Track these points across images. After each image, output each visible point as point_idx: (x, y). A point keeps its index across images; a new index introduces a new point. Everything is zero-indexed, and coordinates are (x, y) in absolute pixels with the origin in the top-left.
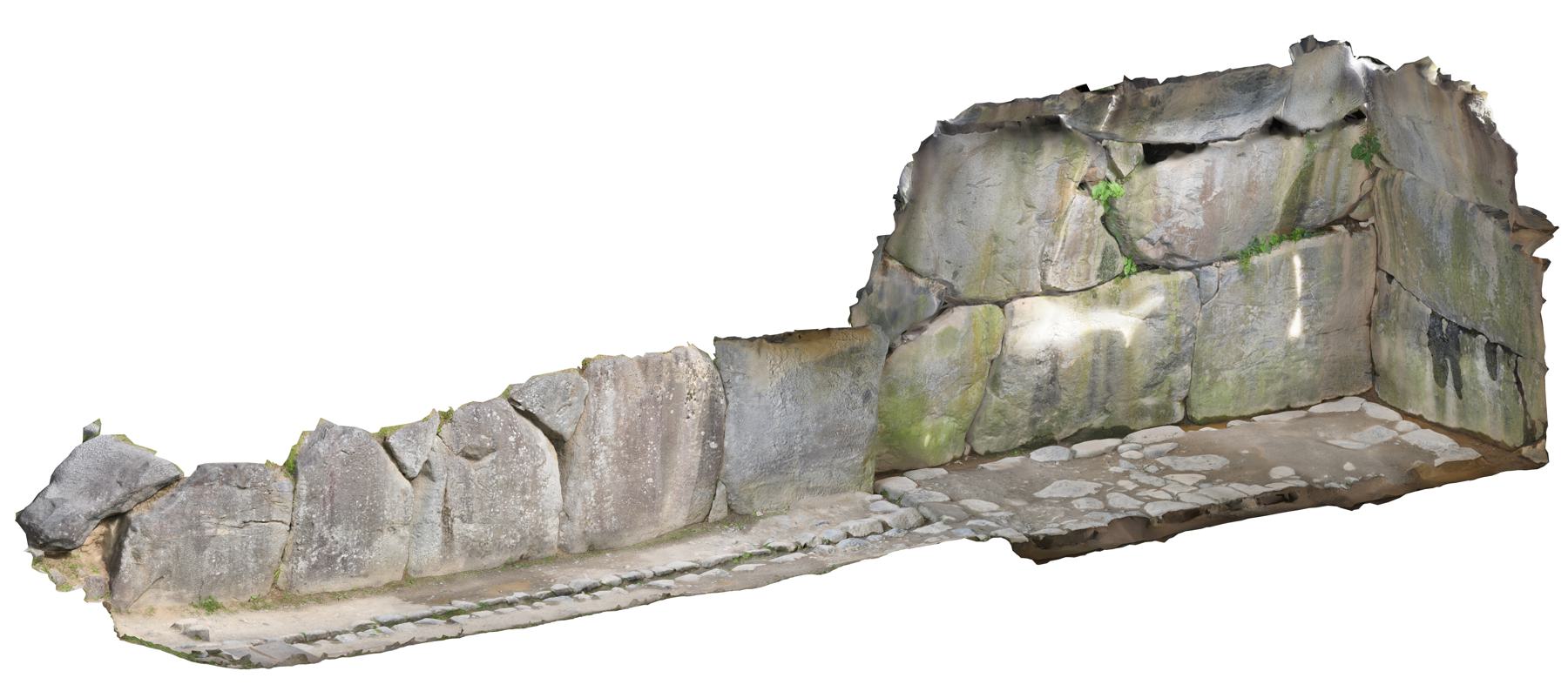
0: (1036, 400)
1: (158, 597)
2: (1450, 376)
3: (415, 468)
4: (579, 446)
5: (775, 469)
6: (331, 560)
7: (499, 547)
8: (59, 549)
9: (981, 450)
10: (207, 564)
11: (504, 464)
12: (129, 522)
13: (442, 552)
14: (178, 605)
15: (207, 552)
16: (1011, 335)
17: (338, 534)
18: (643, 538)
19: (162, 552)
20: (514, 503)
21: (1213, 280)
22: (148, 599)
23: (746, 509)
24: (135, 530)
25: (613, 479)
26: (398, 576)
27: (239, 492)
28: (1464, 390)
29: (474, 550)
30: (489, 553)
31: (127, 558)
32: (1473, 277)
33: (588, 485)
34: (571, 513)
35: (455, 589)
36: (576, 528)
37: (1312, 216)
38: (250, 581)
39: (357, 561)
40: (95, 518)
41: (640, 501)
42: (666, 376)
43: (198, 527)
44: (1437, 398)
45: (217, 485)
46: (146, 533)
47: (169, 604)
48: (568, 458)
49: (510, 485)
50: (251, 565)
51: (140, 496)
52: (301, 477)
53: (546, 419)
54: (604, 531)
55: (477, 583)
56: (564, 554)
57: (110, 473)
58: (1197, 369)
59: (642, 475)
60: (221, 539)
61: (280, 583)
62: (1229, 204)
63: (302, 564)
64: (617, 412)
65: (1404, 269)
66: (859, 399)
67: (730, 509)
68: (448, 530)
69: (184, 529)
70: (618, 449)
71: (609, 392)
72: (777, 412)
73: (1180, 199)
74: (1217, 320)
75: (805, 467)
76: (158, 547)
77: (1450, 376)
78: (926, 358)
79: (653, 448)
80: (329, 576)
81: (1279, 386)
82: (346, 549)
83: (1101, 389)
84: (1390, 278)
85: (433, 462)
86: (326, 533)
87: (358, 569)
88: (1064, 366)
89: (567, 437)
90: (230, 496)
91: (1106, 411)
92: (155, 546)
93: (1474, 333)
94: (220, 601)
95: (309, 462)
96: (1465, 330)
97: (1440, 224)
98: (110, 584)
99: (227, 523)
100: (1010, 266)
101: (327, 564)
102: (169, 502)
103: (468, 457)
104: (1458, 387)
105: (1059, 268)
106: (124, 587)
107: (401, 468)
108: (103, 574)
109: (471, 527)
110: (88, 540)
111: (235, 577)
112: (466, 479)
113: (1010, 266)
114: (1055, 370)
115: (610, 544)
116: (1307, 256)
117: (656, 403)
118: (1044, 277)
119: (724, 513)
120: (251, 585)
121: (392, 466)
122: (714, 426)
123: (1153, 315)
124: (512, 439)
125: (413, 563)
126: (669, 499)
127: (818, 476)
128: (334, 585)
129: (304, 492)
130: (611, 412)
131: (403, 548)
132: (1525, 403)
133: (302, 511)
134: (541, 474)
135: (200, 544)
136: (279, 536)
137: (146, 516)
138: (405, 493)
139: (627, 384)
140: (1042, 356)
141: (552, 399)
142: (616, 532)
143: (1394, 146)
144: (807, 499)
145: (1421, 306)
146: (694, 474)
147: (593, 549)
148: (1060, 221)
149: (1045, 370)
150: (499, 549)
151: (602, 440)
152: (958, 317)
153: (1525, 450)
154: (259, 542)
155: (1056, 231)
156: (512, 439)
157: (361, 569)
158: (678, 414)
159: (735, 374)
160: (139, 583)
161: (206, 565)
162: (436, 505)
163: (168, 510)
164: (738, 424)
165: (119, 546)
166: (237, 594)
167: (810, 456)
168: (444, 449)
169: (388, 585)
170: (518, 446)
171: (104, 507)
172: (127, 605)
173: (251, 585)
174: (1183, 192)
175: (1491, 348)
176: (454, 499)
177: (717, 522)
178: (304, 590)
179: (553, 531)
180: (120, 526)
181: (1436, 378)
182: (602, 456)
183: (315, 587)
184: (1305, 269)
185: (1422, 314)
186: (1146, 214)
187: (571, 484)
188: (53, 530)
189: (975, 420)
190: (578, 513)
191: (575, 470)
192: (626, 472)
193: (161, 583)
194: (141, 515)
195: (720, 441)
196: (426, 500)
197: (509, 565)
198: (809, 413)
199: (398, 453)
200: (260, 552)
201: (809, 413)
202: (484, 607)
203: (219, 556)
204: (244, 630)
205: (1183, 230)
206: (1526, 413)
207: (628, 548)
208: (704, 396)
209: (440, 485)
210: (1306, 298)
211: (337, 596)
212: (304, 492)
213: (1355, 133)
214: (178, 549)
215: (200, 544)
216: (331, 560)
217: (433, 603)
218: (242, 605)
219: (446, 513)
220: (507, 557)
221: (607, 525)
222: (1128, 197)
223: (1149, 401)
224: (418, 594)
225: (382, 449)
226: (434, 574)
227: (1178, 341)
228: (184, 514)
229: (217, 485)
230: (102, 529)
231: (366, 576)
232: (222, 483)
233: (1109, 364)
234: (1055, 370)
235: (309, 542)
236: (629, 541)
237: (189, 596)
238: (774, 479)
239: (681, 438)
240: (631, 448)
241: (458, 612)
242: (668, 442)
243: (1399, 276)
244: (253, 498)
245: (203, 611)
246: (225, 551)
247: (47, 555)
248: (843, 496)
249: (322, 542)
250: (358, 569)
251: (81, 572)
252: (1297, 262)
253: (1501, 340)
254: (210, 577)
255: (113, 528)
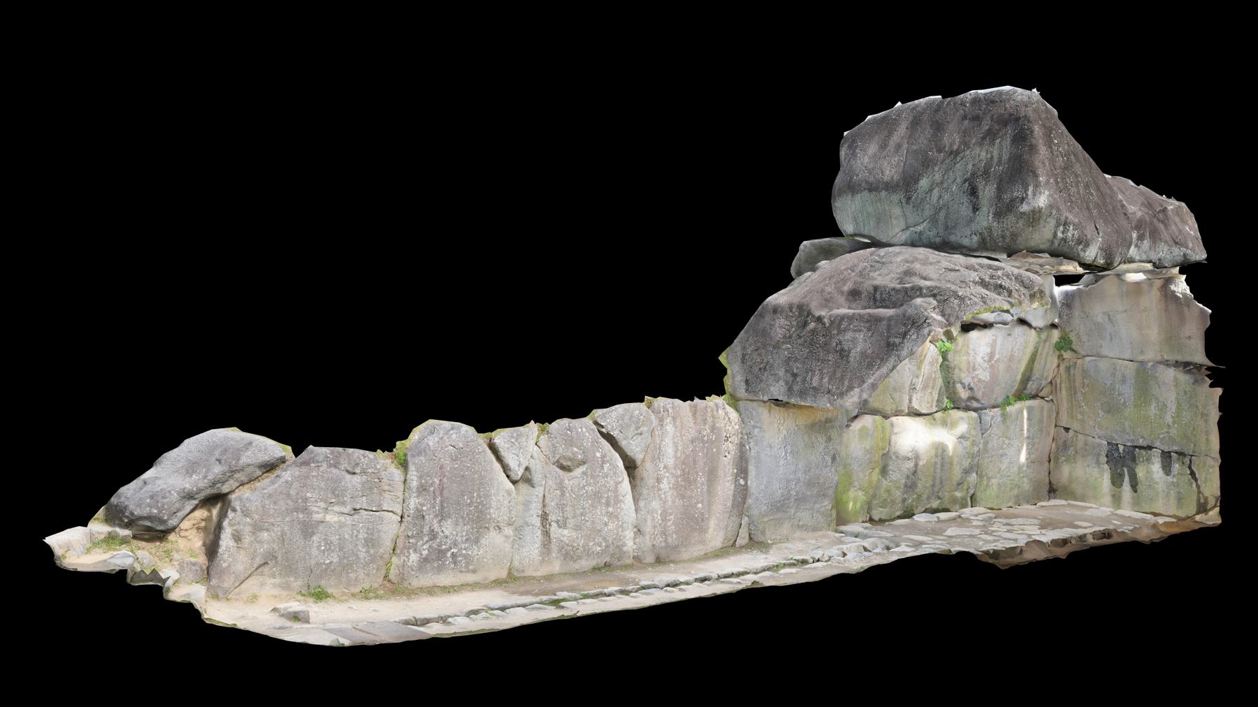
0: (906, 486)
1: (262, 585)
2: (1127, 478)
3: (518, 472)
4: (647, 470)
5: (778, 507)
6: (441, 553)
7: (588, 553)
8: (149, 529)
9: (876, 518)
10: (315, 550)
11: (593, 477)
12: (230, 502)
13: (542, 554)
14: (285, 593)
15: (314, 538)
16: (893, 438)
17: (448, 528)
18: (695, 554)
19: (265, 535)
20: (600, 514)
21: (989, 418)
22: (251, 585)
23: (761, 539)
24: (234, 510)
25: (673, 502)
26: (503, 574)
27: (348, 477)
28: (1139, 487)
29: (568, 554)
30: (580, 558)
31: (226, 541)
32: (1153, 410)
33: (655, 504)
34: (643, 529)
35: (555, 586)
36: (647, 541)
37: (1032, 387)
38: (361, 572)
39: (466, 556)
40: (190, 496)
41: (693, 523)
42: (710, 420)
43: (305, 510)
44: (1113, 496)
45: (324, 467)
46: (246, 513)
47: (275, 592)
48: (638, 482)
49: (597, 496)
50: (362, 555)
51: (242, 477)
52: (412, 468)
53: (623, 443)
54: (667, 546)
55: (573, 582)
56: (638, 562)
57: (211, 453)
58: (980, 476)
59: (694, 501)
60: (330, 525)
61: (392, 576)
62: (1002, 367)
63: (414, 557)
64: (676, 445)
65: (1082, 421)
66: (829, 459)
67: (751, 538)
68: (546, 534)
69: (290, 511)
70: (677, 477)
71: (670, 428)
72: (782, 462)
73: (979, 360)
74: (990, 446)
75: (798, 508)
76: (261, 529)
77: (1127, 478)
78: (853, 445)
79: (702, 479)
80: (440, 570)
81: (1016, 492)
82: (455, 544)
83: (938, 482)
84: (1067, 429)
85: (533, 468)
86: (436, 527)
87: (467, 564)
88: (921, 463)
89: (639, 463)
90: (338, 480)
91: (939, 498)
92: (257, 528)
93: (1150, 448)
94: (330, 591)
95: (419, 454)
96: (1141, 448)
97: (1124, 381)
98: (208, 568)
99: (336, 508)
100: (895, 389)
101: (437, 557)
102: (273, 483)
103: (563, 468)
104: (1134, 486)
105: (920, 395)
106: (223, 572)
107: (505, 468)
108: (202, 559)
109: (566, 532)
110: (186, 524)
111: (346, 566)
112: (561, 487)
113: (895, 389)
114: (916, 465)
115: (672, 557)
116: (1030, 410)
117: (703, 442)
118: (910, 401)
119: (746, 540)
120: (362, 576)
121: (497, 466)
122: (742, 469)
123: (962, 437)
124: (598, 455)
125: (516, 563)
126: (712, 523)
127: (805, 516)
128: (445, 579)
129: (414, 484)
130: (671, 445)
131: (508, 547)
132: (1198, 487)
133: (413, 502)
134: (620, 490)
135: (308, 529)
136: (390, 527)
137: (247, 495)
138: (509, 493)
139: (682, 423)
140: (910, 455)
141: (628, 426)
142: (677, 546)
143: (1084, 338)
144: (798, 534)
145: (1097, 440)
146: (729, 504)
147: (659, 561)
148: (922, 362)
149: (911, 465)
150: (589, 555)
151: (665, 467)
152: (867, 420)
153: (1198, 518)
154: (371, 532)
155: (919, 368)
156: (598, 455)
157: (469, 565)
158: (718, 452)
159: (754, 427)
160: (239, 567)
161: (315, 552)
162: (536, 509)
163: (270, 489)
164: (757, 467)
165: (219, 527)
166: (348, 585)
167: (801, 500)
168: (542, 457)
169: (495, 581)
170: (603, 462)
171: (201, 485)
172: (227, 592)
173: (362, 576)
174: (981, 355)
175: (1166, 457)
176: (552, 504)
177: (742, 547)
178: (416, 583)
179: (630, 545)
180: (221, 509)
181: (1113, 483)
182: (665, 481)
183: (427, 580)
184: (1029, 419)
185: (1100, 445)
186: (964, 366)
187: (642, 504)
188: (139, 506)
189: (874, 496)
190: (648, 528)
191: (645, 492)
192: (683, 497)
193: (266, 569)
194: (243, 497)
195: (746, 479)
196: (527, 504)
197: (596, 569)
198: (800, 466)
199: (503, 453)
200: (371, 542)
201: (800, 466)
202: (586, 597)
203: (328, 543)
204: (351, 615)
205: (980, 380)
206: (1199, 492)
207: (684, 561)
208: (735, 440)
209: (539, 491)
210: (1028, 437)
211: (447, 590)
212: (414, 484)
213: (1056, 334)
214: (283, 534)
215: (308, 529)
216: (441, 553)
217: (537, 595)
218: (353, 595)
219: (544, 517)
220: (593, 563)
221: (670, 540)
222: (956, 352)
223: (958, 494)
224: (522, 589)
225: (489, 452)
226: (535, 574)
227: (973, 456)
228: (289, 495)
229: (324, 467)
230: (201, 514)
231: (474, 571)
232: (330, 466)
233: (942, 465)
234: (916, 465)
235: (419, 535)
236: (685, 556)
237: (297, 584)
238: (779, 515)
239: (721, 473)
240: (686, 481)
241: (564, 600)
242: (712, 475)
243: (1075, 426)
244: (363, 484)
245: (312, 599)
246: (334, 539)
247: (135, 537)
248: (820, 533)
249: (433, 535)
250: (467, 564)
251: (176, 556)
252: (1025, 413)
253: (1175, 448)
254: (318, 564)
255: (215, 512)
